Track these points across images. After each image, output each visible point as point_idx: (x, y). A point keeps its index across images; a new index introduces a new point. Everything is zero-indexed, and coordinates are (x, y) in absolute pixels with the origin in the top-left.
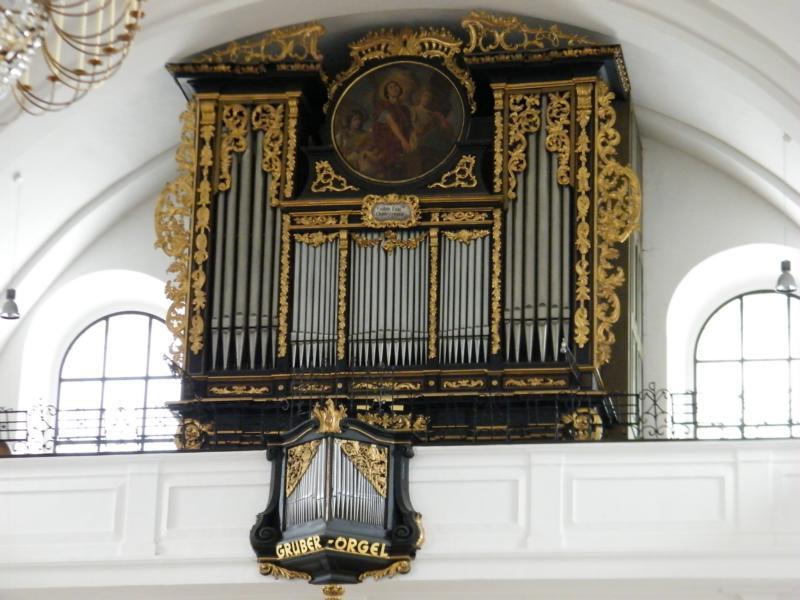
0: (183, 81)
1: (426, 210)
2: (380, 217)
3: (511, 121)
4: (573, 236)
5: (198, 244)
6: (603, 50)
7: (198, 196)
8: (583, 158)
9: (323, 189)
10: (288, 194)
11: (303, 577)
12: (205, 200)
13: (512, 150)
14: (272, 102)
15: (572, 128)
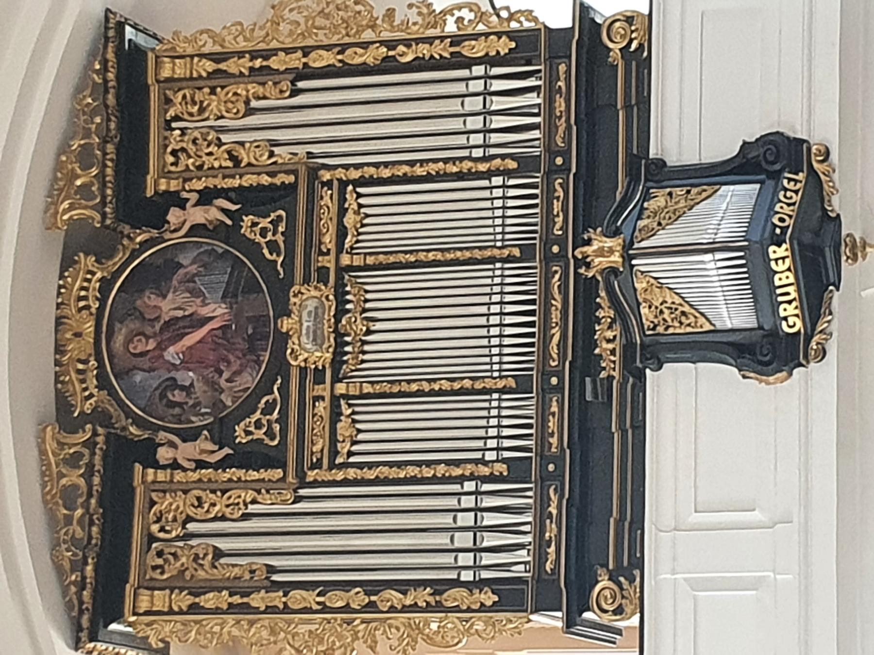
1: (314, 275)
2: (317, 340)
3: (200, 168)
4: (364, 70)
5: (340, 604)
6: (111, 33)
7: (270, 610)
8: (258, 63)
9: (277, 427)
10: (278, 473)
12: (277, 598)
13: (241, 161)
15: (214, 83)
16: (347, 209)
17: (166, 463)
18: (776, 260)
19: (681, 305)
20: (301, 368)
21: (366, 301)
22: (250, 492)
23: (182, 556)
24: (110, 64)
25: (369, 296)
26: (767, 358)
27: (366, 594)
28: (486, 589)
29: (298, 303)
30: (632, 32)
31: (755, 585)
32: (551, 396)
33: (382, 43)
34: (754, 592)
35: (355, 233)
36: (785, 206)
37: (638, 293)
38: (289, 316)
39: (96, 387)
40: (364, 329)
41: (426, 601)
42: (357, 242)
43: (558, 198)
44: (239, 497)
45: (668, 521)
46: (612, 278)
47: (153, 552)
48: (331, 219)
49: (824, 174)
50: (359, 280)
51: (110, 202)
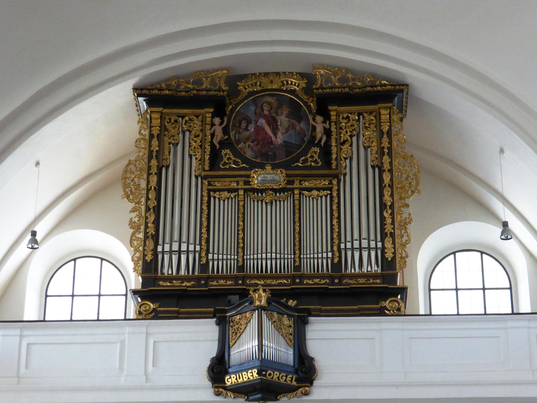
0: (141, 99)
1: (291, 179)
2: (263, 181)
3: (341, 128)
4: (382, 196)
5: (150, 196)
6: (398, 87)
7: (149, 168)
8: (386, 150)
10: (207, 168)
11: (241, 397)
12: (154, 170)
14: (195, 114)
16: (320, 191)
17: (213, 121)
18: (252, 373)
19: (240, 332)
20: (250, 175)
21: (280, 201)
22: (200, 157)
23: (174, 130)
24: (384, 88)
25: (282, 202)
26: (215, 371)
27: (153, 207)
28: (153, 256)
29: (278, 173)
30: (393, 311)
31: (121, 368)
32: (234, 281)
33: (393, 203)
34: (118, 367)
35: (309, 195)
36: (277, 376)
37: (245, 313)
38: (272, 169)
39: (249, 91)
40: (267, 201)
41: (149, 232)
42: (306, 197)
43: (320, 281)
44: (198, 153)
45: (152, 330)
46: (249, 302)
47: (176, 118)
48: (315, 185)
49: (297, 393)
50: (289, 198)
51: (323, 91)
